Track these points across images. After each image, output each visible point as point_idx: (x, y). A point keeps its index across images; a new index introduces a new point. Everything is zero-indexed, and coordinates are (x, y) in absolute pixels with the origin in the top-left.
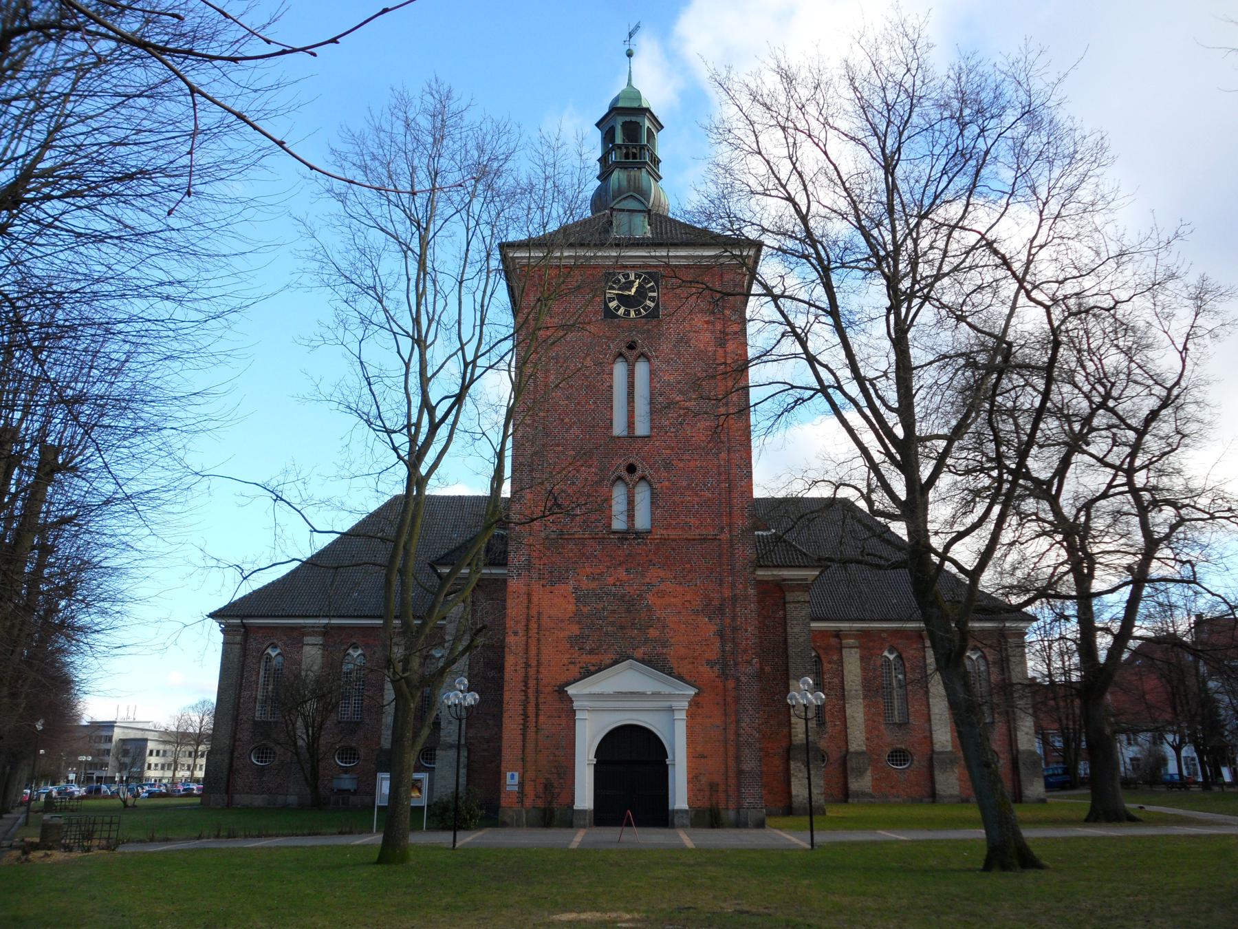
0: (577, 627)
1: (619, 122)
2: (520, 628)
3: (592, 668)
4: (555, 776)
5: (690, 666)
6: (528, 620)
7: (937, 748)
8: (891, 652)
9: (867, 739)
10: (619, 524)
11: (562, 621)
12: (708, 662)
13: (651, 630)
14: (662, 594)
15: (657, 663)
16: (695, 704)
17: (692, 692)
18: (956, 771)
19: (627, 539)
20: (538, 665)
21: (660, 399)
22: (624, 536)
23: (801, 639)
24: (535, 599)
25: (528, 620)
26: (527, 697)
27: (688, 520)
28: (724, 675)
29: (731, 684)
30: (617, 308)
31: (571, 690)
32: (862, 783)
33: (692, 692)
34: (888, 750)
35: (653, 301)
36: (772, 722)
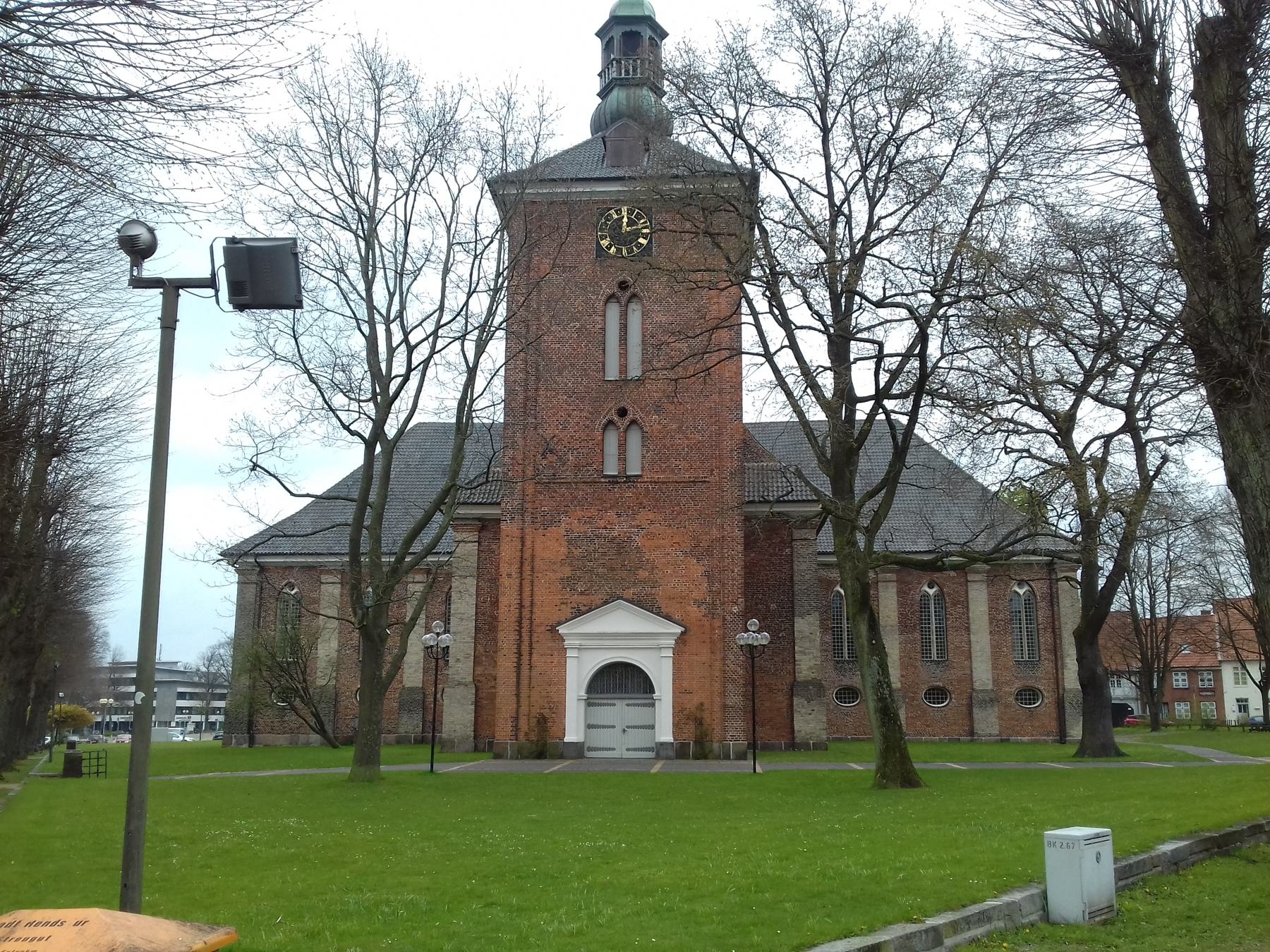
0: (569, 569)
1: (617, 33)
2: (514, 570)
3: (583, 609)
4: (547, 710)
5: (678, 606)
6: (522, 563)
7: (977, 685)
8: (931, 587)
9: (902, 676)
10: (611, 469)
11: (554, 563)
12: (695, 601)
13: (640, 572)
14: (651, 536)
15: (647, 604)
16: (681, 640)
17: (679, 630)
18: (996, 709)
19: (617, 483)
20: (532, 603)
21: (652, 341)
22: (613, 480)
23: (807, 577)
24: (528, 543)
25: (522, 563)
26: (521, 636)
27: (678, 462)
28: (711, 614)
29: (717, 623)
30: (609, 248)
31: (562, 630)
32: (988, 722)
33: (679, 630)
34: (925, 688)
35: (646, 239)
36: (776, 659)
